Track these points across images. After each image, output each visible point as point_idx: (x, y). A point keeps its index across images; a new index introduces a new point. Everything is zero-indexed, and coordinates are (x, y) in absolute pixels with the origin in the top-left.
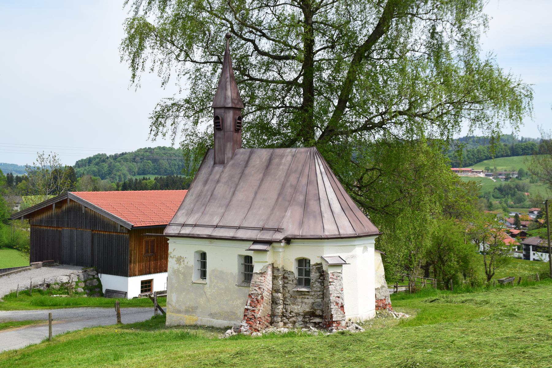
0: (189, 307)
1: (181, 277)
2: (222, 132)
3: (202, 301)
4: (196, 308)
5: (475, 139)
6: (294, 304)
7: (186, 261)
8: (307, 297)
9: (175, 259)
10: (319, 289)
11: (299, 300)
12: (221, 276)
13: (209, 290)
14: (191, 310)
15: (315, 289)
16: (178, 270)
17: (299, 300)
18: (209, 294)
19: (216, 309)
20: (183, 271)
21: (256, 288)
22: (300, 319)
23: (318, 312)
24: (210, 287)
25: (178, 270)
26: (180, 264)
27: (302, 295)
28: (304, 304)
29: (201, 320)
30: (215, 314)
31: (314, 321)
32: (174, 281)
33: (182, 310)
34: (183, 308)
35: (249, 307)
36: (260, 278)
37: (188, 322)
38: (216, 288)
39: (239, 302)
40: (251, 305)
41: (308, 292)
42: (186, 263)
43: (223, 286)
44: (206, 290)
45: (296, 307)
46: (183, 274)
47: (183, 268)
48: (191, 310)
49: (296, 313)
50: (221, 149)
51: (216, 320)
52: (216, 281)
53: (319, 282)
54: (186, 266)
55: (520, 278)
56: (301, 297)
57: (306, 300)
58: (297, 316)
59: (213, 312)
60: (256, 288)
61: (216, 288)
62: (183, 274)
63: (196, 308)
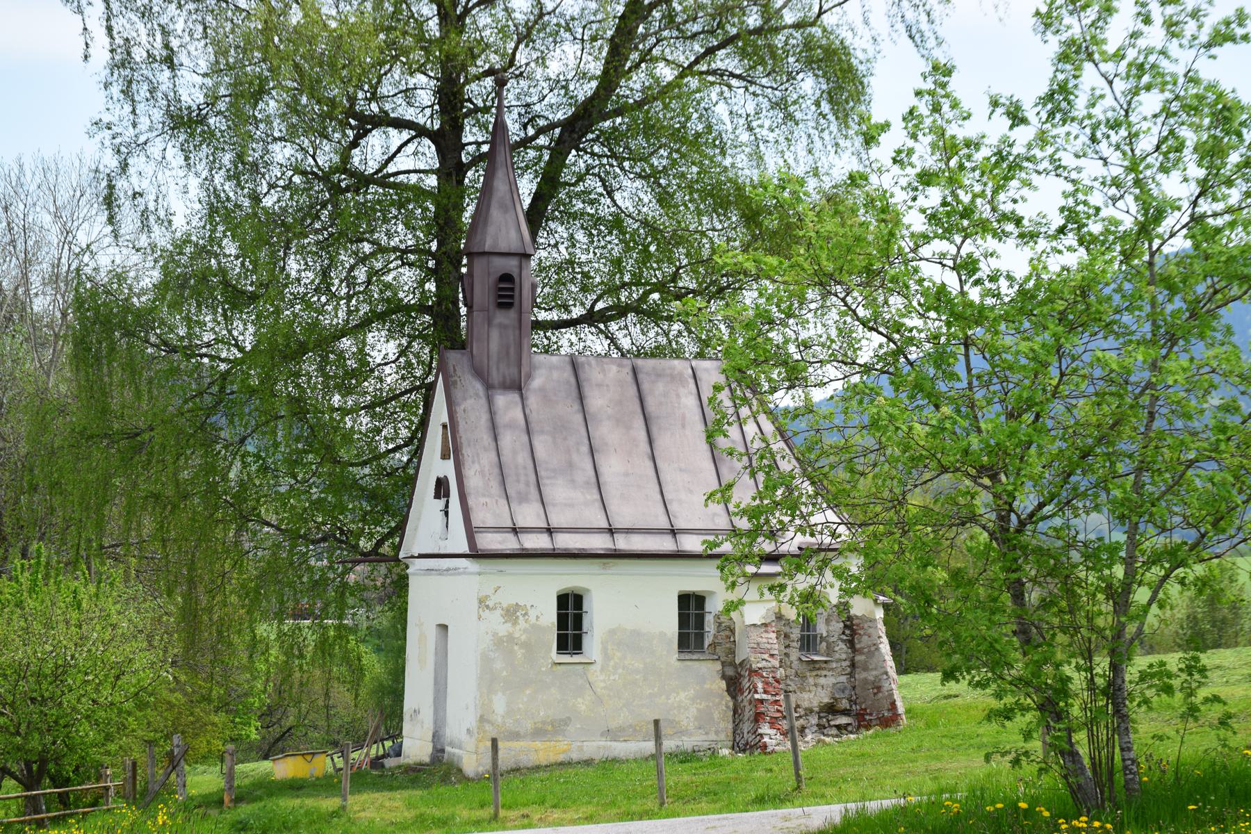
0: (544, 723)
1: (519, 652)
2: (512, 314)
3: (583, 704)
4: (566, 721)
5: (453, 213)
6: (802, 689)
7: (532, 614)
8: (824, 673)
9: (499, 612)
10: (844, 656)
11: (811, 680)
12: (629, 641)
13: (602, 678)
14: (550, 728)
15: (837, 656)
16: (510, 638)
17: (811, 680)
18: (602, 685)
19: (622, 718)
20: (523, 637)
21: (766, 656)
22: (814, 720)
23: (844, 704)
24: (602, 670)
25: (510, 638)
26: (515, 623)
27: (815, 669)
28: (820, 689)
29: (580, 749)
30: (621, 729)
31: (837, 722)
32: (498, 665)
33: (522, 732)
34: (529, 725)
35: (765, 696)
36: (765, 635)
37: (543, 758)
38: (620, 671)
39: (683, 695)
40: (765, 692)
41: (826, 662)
42: (532, 619)
43: (639, 665)
44: (592, 679)
45: (806, 695)
46: (526, 645)
47: (525, 631)
48: (550, 728)
49: (806, 709)
50: (508, 353)
51: (624, 744)
52: (619, 654)
53: (843, 641)
54: (533, 626)
55: (656, 722)
56: (814, 673)
57: (822, 681)
58: (806, 715)
59: (613, 725)
60: (766, 656)
61: (620, 671)
62: (526, 645)
63: (566, 721)
